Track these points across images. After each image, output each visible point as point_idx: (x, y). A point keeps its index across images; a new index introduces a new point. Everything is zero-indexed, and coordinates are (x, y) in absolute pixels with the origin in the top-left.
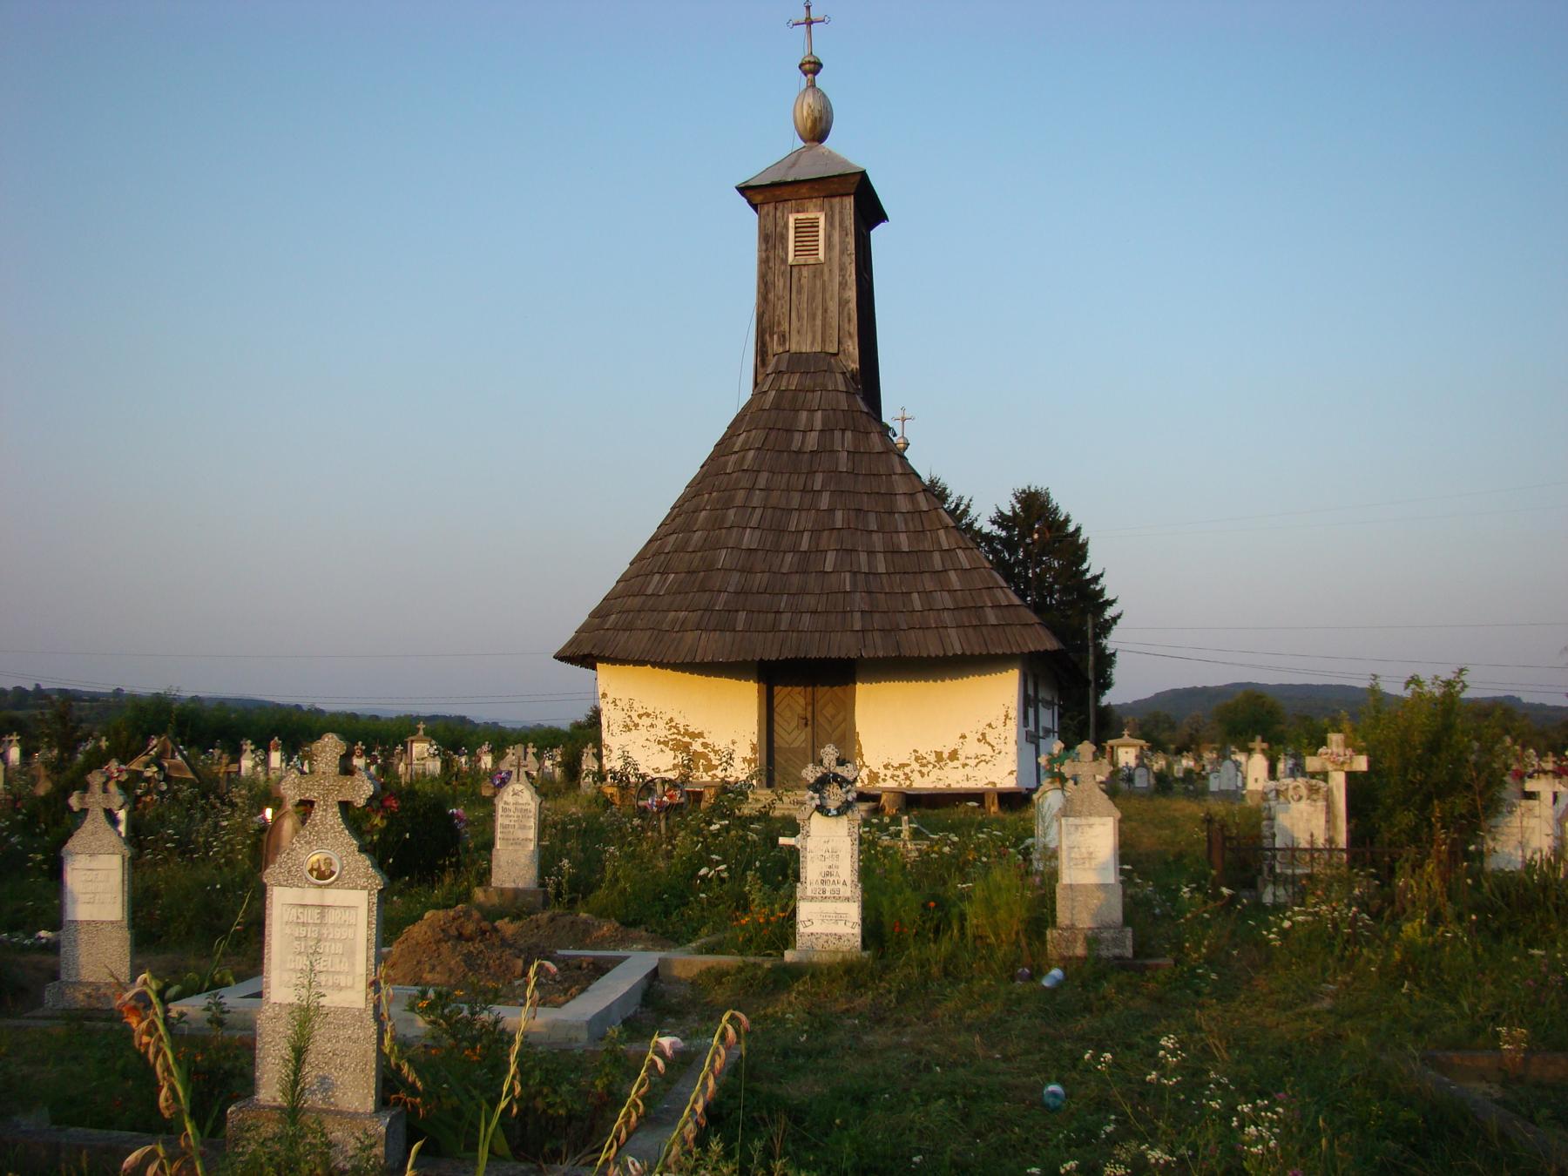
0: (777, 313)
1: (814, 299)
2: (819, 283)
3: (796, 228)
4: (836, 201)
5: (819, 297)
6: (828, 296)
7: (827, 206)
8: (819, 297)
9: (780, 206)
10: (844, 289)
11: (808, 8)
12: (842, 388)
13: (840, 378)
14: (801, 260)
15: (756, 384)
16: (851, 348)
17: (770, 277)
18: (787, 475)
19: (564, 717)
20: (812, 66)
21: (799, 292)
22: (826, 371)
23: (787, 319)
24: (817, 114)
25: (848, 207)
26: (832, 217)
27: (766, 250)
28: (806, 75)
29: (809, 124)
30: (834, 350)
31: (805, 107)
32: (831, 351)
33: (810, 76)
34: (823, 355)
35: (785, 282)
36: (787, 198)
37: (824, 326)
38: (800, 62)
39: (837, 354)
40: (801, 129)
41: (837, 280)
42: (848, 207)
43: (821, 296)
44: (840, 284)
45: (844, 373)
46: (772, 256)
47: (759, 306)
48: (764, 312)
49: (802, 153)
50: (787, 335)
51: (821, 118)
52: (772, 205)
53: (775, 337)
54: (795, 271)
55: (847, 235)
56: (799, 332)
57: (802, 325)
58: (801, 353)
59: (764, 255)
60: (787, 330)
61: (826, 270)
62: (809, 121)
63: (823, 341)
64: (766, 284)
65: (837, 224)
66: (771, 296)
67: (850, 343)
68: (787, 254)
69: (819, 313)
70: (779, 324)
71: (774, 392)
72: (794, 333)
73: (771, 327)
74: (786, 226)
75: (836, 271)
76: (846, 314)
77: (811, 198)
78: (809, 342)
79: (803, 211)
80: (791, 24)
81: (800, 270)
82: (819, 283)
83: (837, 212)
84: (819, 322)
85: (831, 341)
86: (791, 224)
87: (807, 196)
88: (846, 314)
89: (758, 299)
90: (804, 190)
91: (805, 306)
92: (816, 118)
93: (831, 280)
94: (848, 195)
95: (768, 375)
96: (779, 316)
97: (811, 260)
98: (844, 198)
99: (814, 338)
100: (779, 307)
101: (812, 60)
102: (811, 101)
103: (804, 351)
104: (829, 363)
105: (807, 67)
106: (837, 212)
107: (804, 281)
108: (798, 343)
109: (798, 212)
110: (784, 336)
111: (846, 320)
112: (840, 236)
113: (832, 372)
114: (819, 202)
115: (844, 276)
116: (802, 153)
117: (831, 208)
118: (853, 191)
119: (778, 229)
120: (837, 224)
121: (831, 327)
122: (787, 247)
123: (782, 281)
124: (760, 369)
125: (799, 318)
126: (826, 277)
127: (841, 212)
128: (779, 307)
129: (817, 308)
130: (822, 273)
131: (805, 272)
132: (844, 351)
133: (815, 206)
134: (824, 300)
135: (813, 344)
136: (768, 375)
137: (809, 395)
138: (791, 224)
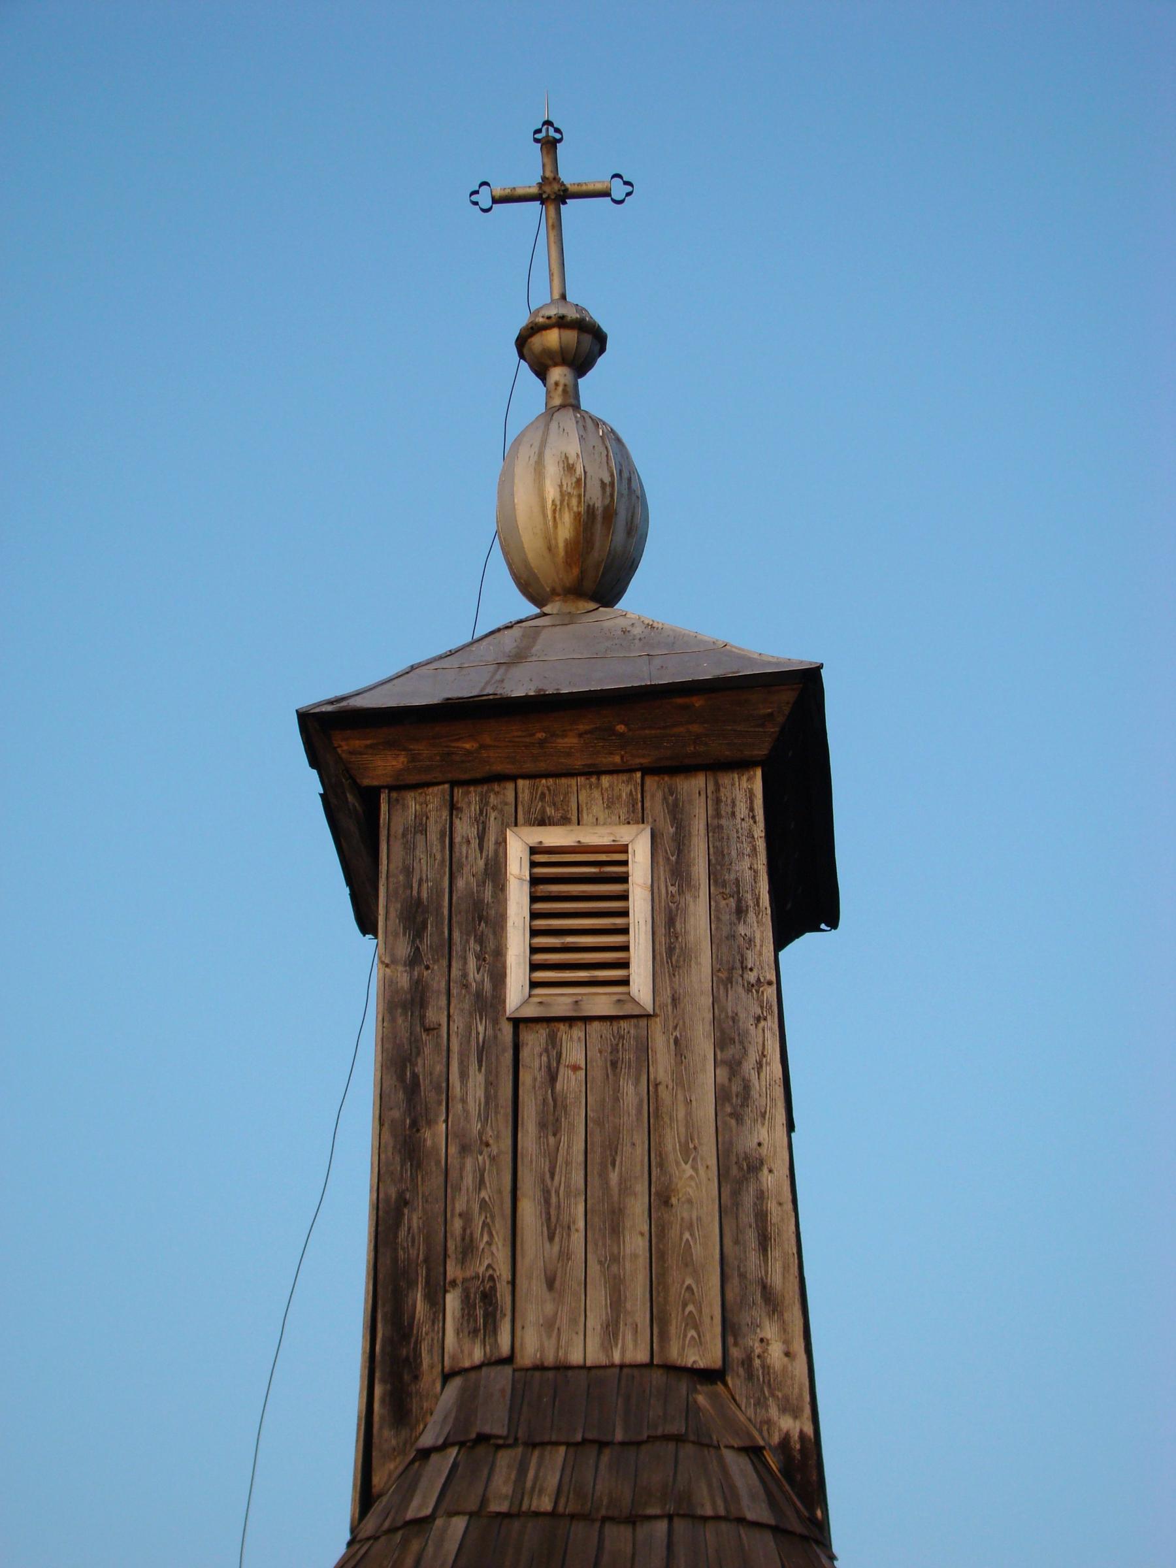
0: (460, 1206)
1: (612, 1148)
2: (631, 1093)
3: (535, 881)
4: (694, 786)
5: (634, 1153)
6: (671, 1142)
7: (656, 806)
8: (634, 1153)
9: (470, 800)
10: (738, 1117)
11: (550, 146)
12: (756, 1511)
13: (740, 1469)
14: (561, 1002)
15: (366, 1497)
16: (776, 1351)
17: (428, 1063)
18: (662, 1526)
19: (628, 991)
20: (571, 336)
21: (551, 1124)
22: (678, 1439)
23: (501, 1229)
24: (595, 495)
25: (742, 809)
26: (681, 842)
27: (414, 960)
28: (541, 373)
29: (565, 531)
30: (707, 1355)
31: (552, 471)
32: (693, 1358)
33: (558, 374)
34: (657, 1378)
35: (489, 1084)
36: (499, 768)
37: (657, 1255)
38: (522, 321)
39: (711, 1376)
40: (531, 543)
41: (707, 1079)
42: (742, 809)
43: (640, 1138)
44: (722, 1096)
45: (754, 1452)
46: (438, 983)
47: (382, 1176)
48: (403, 1202)
49: (538, 630)
50: (503, 1292)
51: (609, 514)
52: (435, 797)
53: (452, 1301)
54: (534, 1040)
55: (740, 912)
56: (550, 1283)
57: (565, 1255)
58: (563, 1368)
59: (404, 980)
60: (504, 1272)
61: (661, 1044)
62: (567, 519)
63: (659, 1319)
64: (412, 1089)
65: (700, 870)
66: (435, 1135)
67: (770, 1330)
68: (499, 977)
69: (637, 1207)
70: (468, 1249)
71: (459, 1524)
72: (532, 1286)
73: (436, 1260)
74: (495, 872)
75: (703, 1046)
76: (747, 1217)
77: (593, 772)
78: (595, 1322)
79: (564, 821)
80: (484, 199)
81: (553, 1039)
82: (631, 1093)
83: (698, 827)
84: (635, 1244)
85: (693, 1322)
86: (517, 866)
87: (578, 763)
88: (747, 1217)
89: (380, 1149)
90: (571, 741)
91: (577, 1178)
92: (591, 510)
93: (683, 1079)
94: (742, 765)
95: (425, 1454)
96: (466, 1217)
97: (600, 1002)
98: (725, 779)
99: (617, 1303)
100: (469, 1180)
101: (572, 314)
102: (573, 448)
103: (576, 1358)
104: (691, 1410)
105: (552, 338)
106: (698, 827)
107: (570, 1082)
108: (550, 1325)
109: (542, 821)
110: (488, 1297)
111: (751, 1238)
112: (715, 916)
113: (705, 1444)
114: (623, 787)
115: (734, 1067)
116: (538, 630)
117: (677, 813)
118: (762, 751)
119: (460, 883)
120: (700, 870)
121: (687, 1262)
122: (499, 953)
123: (477, 1079)
124: (386, 1436)
125: (553, 1228)
126: (663, 1064)
127: (714, 830)
128: (469, 1180)
129: (625, 1188)
130: (644, 1049)
131: (573, 1048)
132: (747, 1362)
133: (610, 805)
134: (656, 1160)
135: (611, 1331)
136: (425, 1454)
137: (618, 1537)
138: (517, 866)
